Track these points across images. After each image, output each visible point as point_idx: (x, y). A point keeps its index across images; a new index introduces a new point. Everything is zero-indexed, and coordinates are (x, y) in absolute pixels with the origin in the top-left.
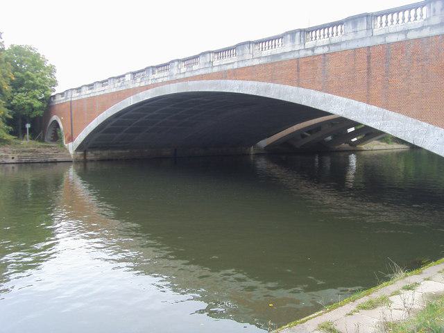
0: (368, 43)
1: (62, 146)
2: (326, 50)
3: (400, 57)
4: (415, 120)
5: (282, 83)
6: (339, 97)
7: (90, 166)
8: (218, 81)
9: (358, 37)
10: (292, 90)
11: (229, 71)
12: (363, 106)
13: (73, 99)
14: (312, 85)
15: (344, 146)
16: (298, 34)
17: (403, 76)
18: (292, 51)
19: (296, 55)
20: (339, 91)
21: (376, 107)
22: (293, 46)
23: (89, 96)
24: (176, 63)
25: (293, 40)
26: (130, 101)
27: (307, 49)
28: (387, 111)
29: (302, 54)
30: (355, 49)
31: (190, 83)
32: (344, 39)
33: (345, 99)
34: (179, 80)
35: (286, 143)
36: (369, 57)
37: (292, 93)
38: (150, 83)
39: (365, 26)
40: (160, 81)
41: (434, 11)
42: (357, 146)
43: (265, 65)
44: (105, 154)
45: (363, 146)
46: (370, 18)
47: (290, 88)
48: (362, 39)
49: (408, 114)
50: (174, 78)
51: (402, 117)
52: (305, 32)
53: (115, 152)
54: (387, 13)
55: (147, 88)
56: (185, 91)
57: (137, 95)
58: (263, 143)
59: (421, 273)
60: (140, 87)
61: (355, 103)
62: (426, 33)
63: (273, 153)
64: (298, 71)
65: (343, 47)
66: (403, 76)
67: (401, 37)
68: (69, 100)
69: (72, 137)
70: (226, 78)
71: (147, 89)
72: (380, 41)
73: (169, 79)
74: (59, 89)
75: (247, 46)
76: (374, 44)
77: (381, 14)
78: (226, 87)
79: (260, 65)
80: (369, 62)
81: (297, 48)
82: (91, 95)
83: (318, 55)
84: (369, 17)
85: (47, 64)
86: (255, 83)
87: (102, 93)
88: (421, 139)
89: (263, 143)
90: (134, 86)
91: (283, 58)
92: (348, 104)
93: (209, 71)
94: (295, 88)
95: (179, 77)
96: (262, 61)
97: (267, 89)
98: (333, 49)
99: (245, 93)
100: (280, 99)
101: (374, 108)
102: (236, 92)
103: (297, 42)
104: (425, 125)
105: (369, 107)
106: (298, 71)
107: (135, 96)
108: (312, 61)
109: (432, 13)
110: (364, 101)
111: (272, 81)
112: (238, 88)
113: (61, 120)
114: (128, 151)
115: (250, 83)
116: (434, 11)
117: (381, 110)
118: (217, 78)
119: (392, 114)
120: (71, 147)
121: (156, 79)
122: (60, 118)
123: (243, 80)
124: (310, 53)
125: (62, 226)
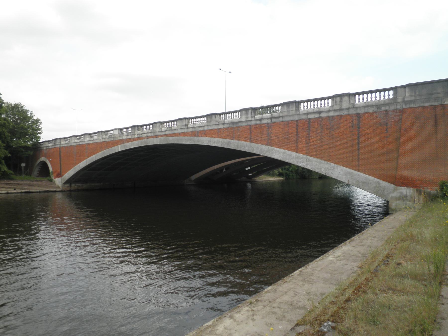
0: (296, 118)
1: (51, 180)
2: (269, 121)
3: (316, 127)
4: (326, 162)
5: (239, 140)
6: (278, 149)
7: (73, 193)
8: (192, 137)
9: (290, 114)
10: (247, 144)
11: (201, 131)
12: (294, 154)
13: (61, 146)
14: (260, 141)
15: (244, 179)
16: (250, 111)
17: (319, 137)
18: (246, 121)
19: (249, 123)
20: (279, 145)
21: (302, 155)
22: (247, 118)
23: (78, 144)
24: (158, 125)
25: (247, 114)
26: (119, 148)
27: (257, 120)
28: (309, 157)
29: (253, 123)
30: (288, 121)
31: (170, 138)
32: (281, 115)
33: (282, 150)
34: (161, 136)
35: (207, 177)
36: (297, 126)
37: (246, 146)
38: (136, 136)
39: (294, 108)
40: (145, 135)
41: (336, 102)
42: (252, 179)
43: (228, 128)
44: (85, 186)
45: (256, 179)
46: (297, 104)
47: (245, 143)
48: (293, 115)
49: (322, 158)
50: (157, 134)
51: (318, 160)
52: (254, 110)
53: (93, 184)
54: (307, 101)
55: (134, 139)
56: (166, 143)
57: (124, 144)
58: (194, 177)
59: (353, 241)
60: (127, 139)
61: (289, 152)
62: (331, 114)
63: (201, 182)
64: (251, 133)
65: (281, 119)
66: (319, 137)
67: (317, 116)
68: (59, 146)
69: (61, 174)
70: (198, 136)
71: (133, 141)
72: (304, 117)
73: (152, 134)
74: (41, 140)
75: (214, 117)
76: (300, 118)
77: (304, 102)
78: (198, 141)
79: (224, 128)
80: (297, 129)
81: (250, 119)
82: (81, 143)
83: (264, 124)
84: (297, 103)
85: (35, 118)
86: (220, 140)
87: (91, 142)
88: (330, 172)
89: (194, 177)
90: (121, 138)
91: (240, 124)
92: (284, 153)
93: (186, 130)
94: (248, 143)
95: (160, 134)
96: (225, 126)
97: (229, 143)
98: (274, 120)
99: (213, 145)
100: (239, 149)
101: (301, 155)
102: (206, 144)
103: (250, 115)
104: (333, 164)
105: (298, 154)
106: (251, 133)
107: (122, 145)
108: (260, 127)
109: (334, 103)
110: (294, 151)
111: (233, 138)
112: (207, 142)
113: (50, 161)
114: (102, 184)
115: (216, 139)
116: (336, 102)
117: (305, 156)
118: (192, 135)
119: (312, 158)
120: (59, 182)
121: (141, 134)
122: (49, 160)
123: (211, 137)
124: (258, 122)
125: (43, 226)
